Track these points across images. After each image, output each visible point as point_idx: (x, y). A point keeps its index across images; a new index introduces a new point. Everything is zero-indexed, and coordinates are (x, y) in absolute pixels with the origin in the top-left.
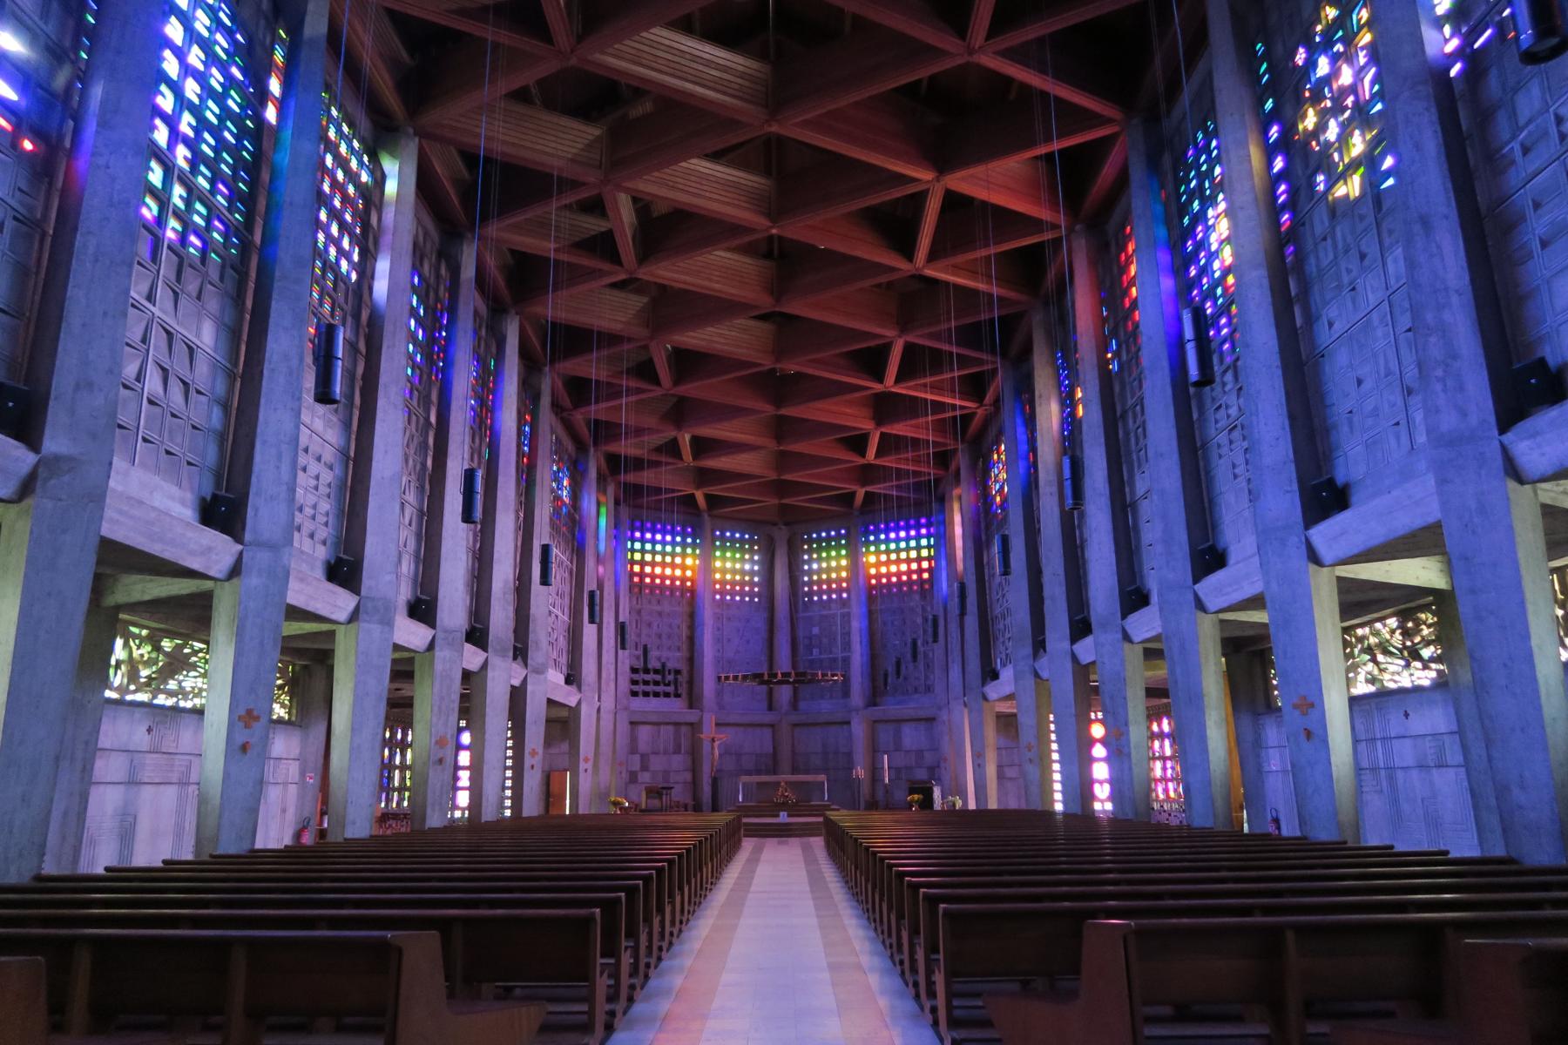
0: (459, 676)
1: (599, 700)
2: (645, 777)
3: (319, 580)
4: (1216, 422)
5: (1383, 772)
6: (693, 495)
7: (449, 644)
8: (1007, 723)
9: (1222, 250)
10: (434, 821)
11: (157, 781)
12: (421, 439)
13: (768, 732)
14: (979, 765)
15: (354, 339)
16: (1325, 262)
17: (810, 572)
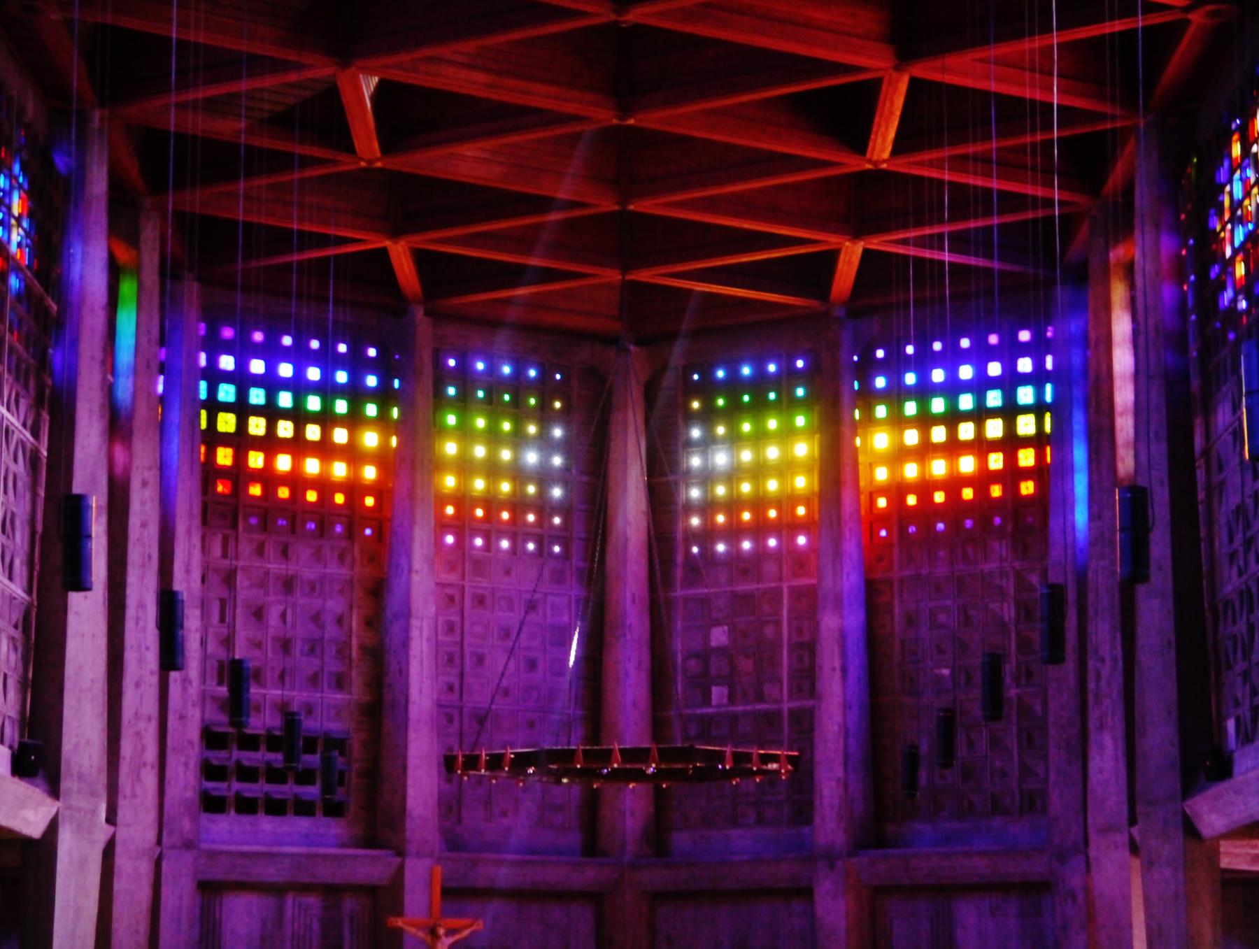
17: (707, 477)
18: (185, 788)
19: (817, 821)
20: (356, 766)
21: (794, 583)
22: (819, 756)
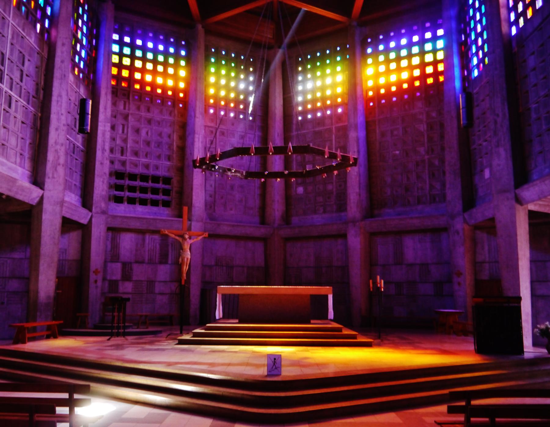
13: (259, 247)
17: (304, 93)
18: (103, 190)
19: (349, 208)
20: (175, 189)
21: (337, 125)
22: (349, 184)
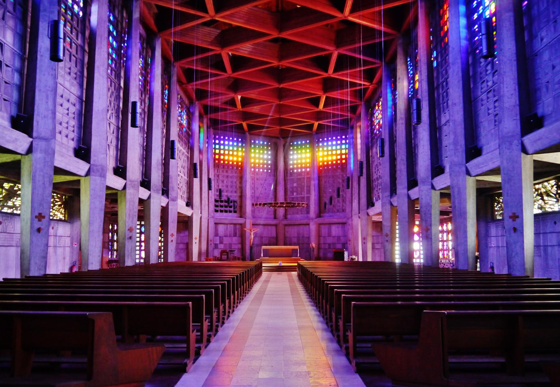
0: (137, 201)
1: (201, 213)
2: (221, 246)
3: (70, 156)
4: (482, 88)
5: (542, 248)
6: (242, 124)
7: (132, 187)
8: (378, 226)
9: (491, 6)
10: (129, 263)
11: (6, 245)
12: (117, 94)
13: (274, 228)
14: (364, 243)
15: (83, 45)
16: (542, 8)
17: (293, 160)
19: (310, 213)
